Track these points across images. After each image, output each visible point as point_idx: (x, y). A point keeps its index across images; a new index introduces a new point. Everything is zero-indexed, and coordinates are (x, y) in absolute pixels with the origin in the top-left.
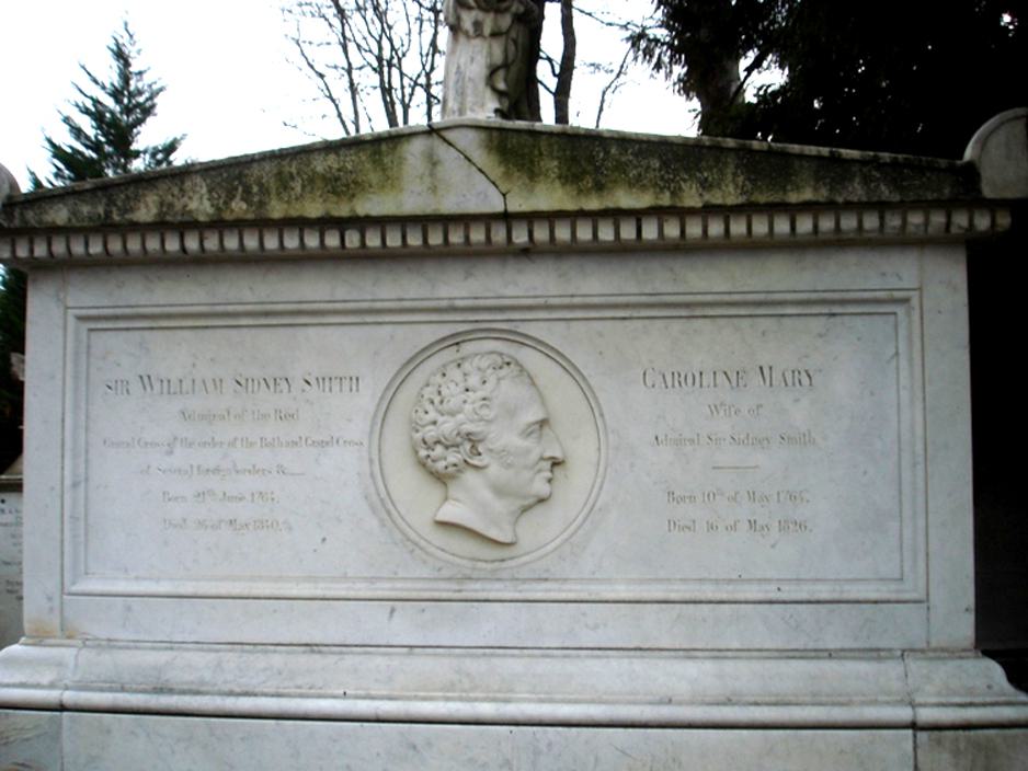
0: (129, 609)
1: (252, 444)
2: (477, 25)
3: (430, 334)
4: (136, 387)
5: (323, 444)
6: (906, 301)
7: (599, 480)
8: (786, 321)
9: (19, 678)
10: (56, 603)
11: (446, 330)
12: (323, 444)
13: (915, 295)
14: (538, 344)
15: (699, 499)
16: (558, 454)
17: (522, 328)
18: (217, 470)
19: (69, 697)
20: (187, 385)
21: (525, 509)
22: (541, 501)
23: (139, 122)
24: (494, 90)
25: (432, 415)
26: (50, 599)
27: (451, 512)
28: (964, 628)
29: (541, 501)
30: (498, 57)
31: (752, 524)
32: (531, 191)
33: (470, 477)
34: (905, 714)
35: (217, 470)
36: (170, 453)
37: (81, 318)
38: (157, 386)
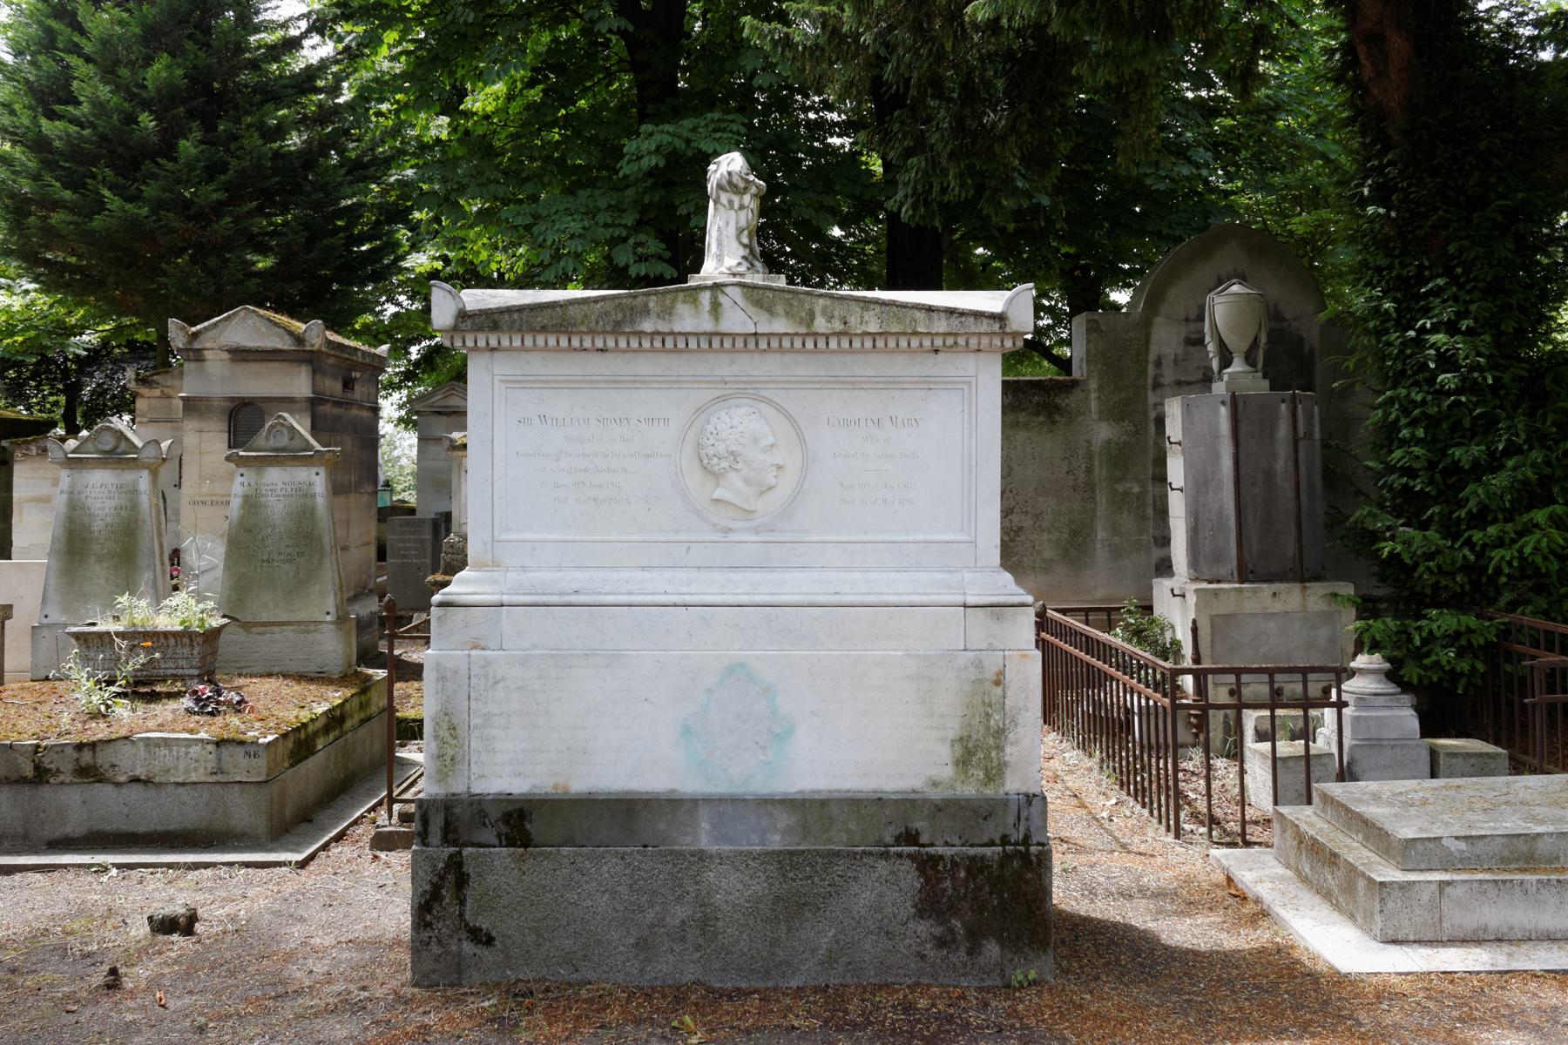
0: (534, 549)
1: (607, 456)
2: (731, 202)
3: (709, 395)
4: (536, 422)
5: (648, 456)
6: (969, 382)
7: (1163, 809)
8: (905, 392)
9: (471, 590)
10: (489, 547)
11: (719, 393)
12: (648, 456)
13: (973, 380)
14: (770, 402)
15: (175, 581)
16: (782, 463)
17: (763, 393)
18: (586, 470)
19: (505, 599)
20: (568, 421)
21: (762, 493)
22: (770, 488)
23: (1332, 904)
24: (741, 243)
25: (712, 441)
26: (485, 544)
27: (719, 493)
28: (997, 559)
29: (770, 488)
30: (743, 223)
31: (885, 501)
32: (770, 322)
33: (733, 476)
34: (959, 599)
35: (586, 470)
36: (558, 460)
37: (500, 381)
38: (549, 421)
